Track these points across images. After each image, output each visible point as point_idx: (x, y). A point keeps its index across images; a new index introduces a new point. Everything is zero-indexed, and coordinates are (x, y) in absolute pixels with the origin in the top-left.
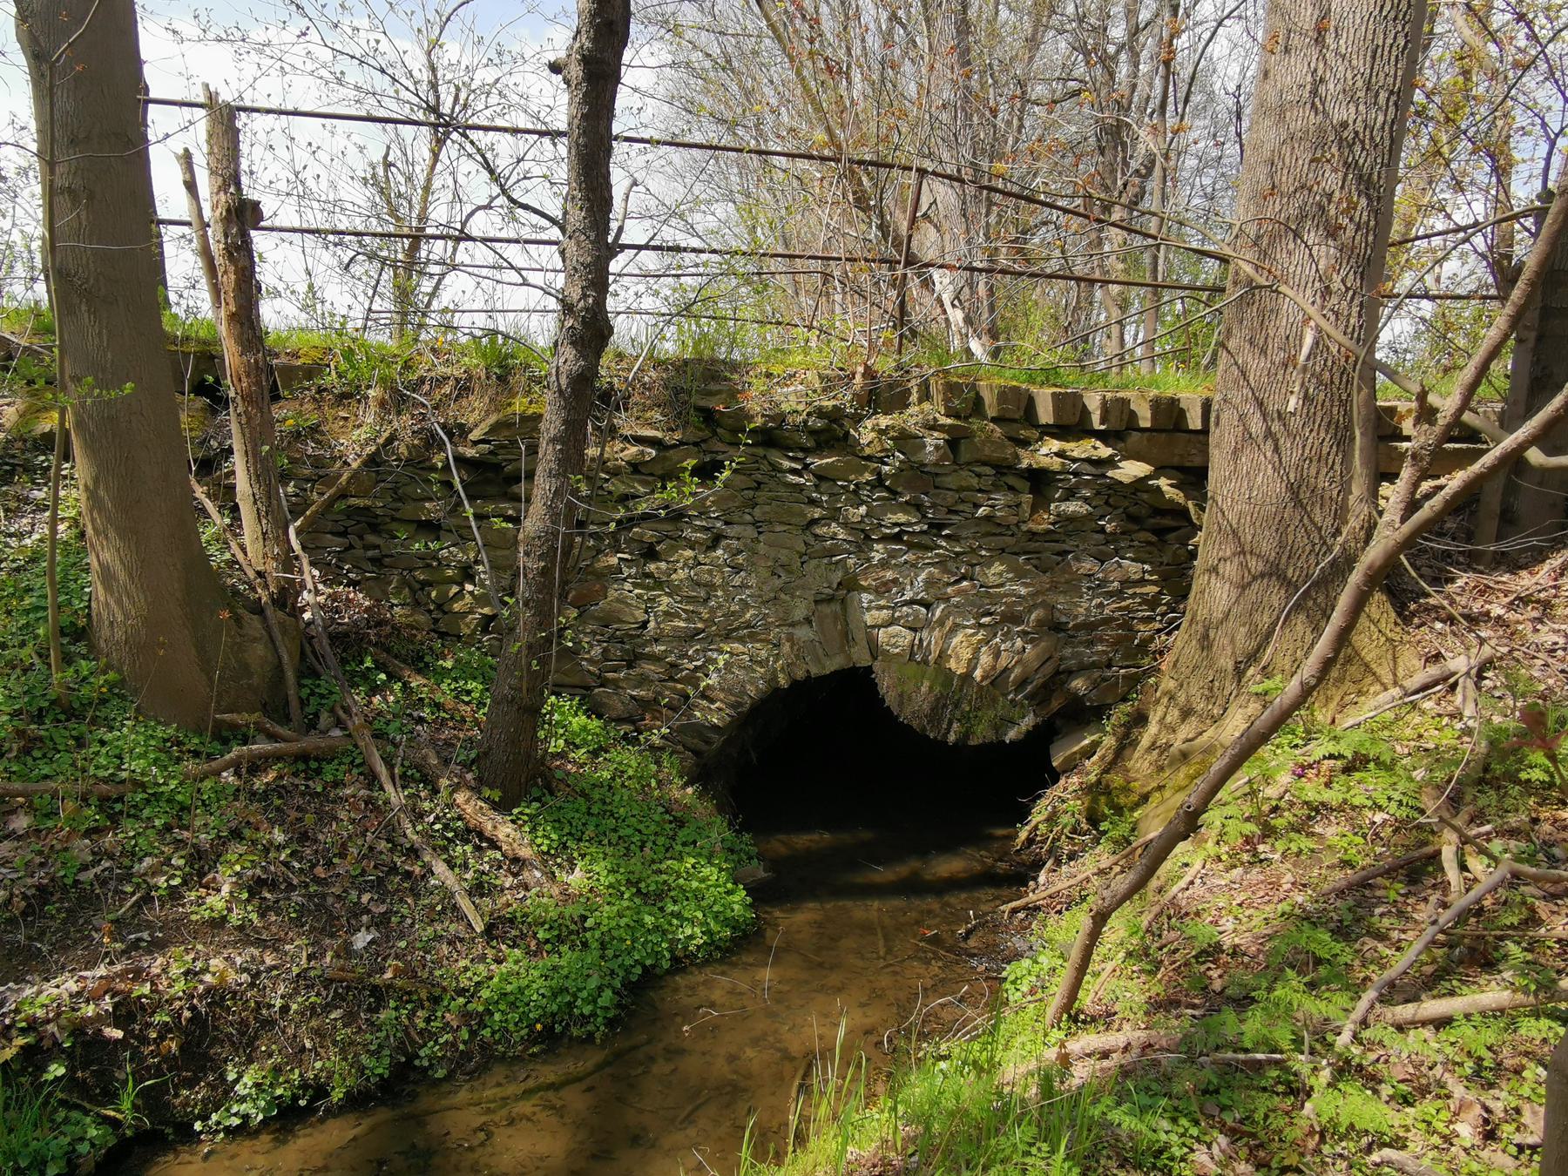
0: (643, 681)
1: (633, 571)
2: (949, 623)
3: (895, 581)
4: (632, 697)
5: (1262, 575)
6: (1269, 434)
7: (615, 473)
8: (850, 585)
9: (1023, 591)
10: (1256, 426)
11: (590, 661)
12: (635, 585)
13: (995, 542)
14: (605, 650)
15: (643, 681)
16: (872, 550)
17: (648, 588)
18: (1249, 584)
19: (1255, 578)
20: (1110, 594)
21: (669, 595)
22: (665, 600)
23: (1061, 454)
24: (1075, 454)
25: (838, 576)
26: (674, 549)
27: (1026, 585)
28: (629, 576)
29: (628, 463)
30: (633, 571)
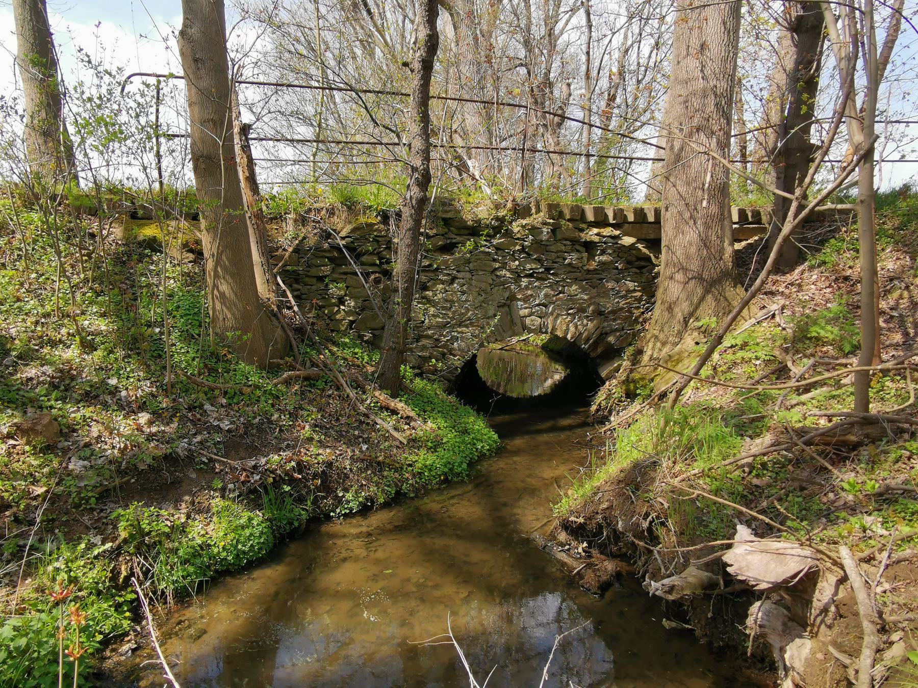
2: (555, 314)
3: (531, 295)
9: (586, 297)
12: (419, 303)
13: (573, 275)
17: (424, 304)
18: (687, 283)
20: (622, 297)
21: (433, 306)
25: (507, 294)
26: (435, 285)
27: (586, 294)
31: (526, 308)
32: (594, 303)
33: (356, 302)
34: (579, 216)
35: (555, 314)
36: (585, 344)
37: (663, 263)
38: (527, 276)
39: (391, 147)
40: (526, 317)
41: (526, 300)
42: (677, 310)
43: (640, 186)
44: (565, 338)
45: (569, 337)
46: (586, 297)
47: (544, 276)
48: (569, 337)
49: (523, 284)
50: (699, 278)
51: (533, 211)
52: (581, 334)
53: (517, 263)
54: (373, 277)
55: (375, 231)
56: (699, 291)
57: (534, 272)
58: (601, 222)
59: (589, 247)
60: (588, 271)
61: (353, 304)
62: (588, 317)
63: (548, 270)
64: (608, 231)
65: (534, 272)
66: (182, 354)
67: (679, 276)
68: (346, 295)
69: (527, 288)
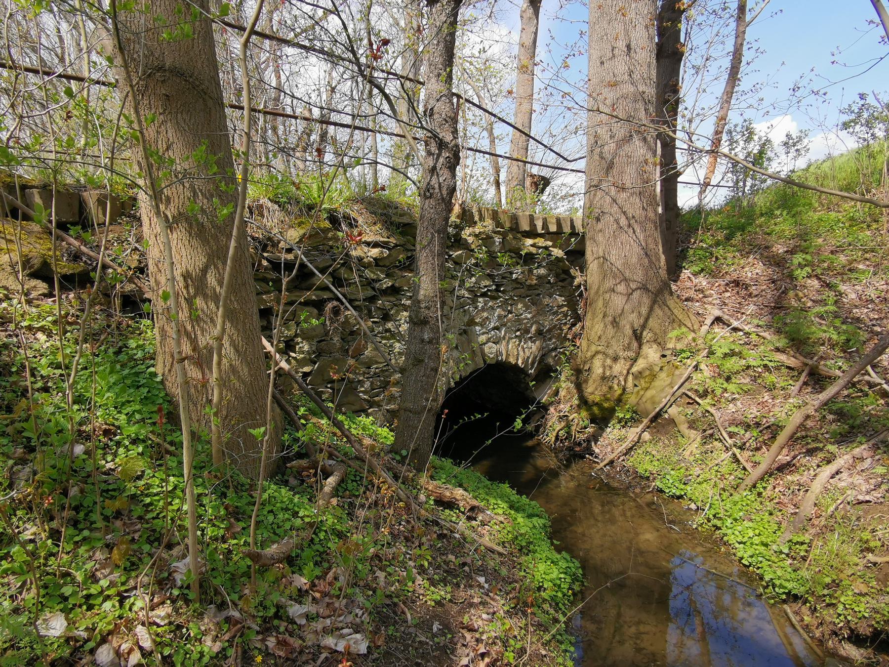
0: (392, 398)
1: (381, 328)
2: (507, 338)
3: (487, 318)
4: (387, 410)
5: (636, 289)
6: (629, 226)
7: (368, 266)
8: (472, 322)
9: (529, 316)
10: (623, 222)
11: (364, 392)
12: (382, 338)
13: (518, 292)
14: (372, 383)
15: (392, 398)
16: (478, 302)
17: (388, 339)
18: (631, 294)
19: (633, 291)
20: (554, 314)
21: (399, 341)
22: (397, 345)
23: (533, 246)
24: (540, 244)
25: (466, 319)
26: (398, 312)
27: (529, 313)
28: (379, 333)
29: (374, 259)
30: (381, 328)
31: (483, 334)
32: (537, 322)
33: (310, 345)
34: (515, 227)
35: (507, 338)
36: (531, 369)
37: (591, 276)
38: (484, 295)
39: (476, 101)
40: (484, 344)
41: (482, 325)
42: (623, 322)
43: (568, 196)
44: (516, 364)
45: (520, 362)
46: (529, 316)
47: (494, 294)
48: (520, 362)
49: (480, 305)
50: (644, 288)
51: (476, 218)
52: (528, 358)
53: (473, 279)
54: (330, 305)
55: (330, 239)
56: (646, 301)
57: (488, 290)
58: (532, 234)
59: (529, 259)
60: (530, 286)
61: (306, 348)
62: (531, 338)
63: (498, 286)
64: (541, 242)
65: (488, 290)
66: (179, 497)
67: (621, 288)
68: (296, 335)
69: (483, 310)
